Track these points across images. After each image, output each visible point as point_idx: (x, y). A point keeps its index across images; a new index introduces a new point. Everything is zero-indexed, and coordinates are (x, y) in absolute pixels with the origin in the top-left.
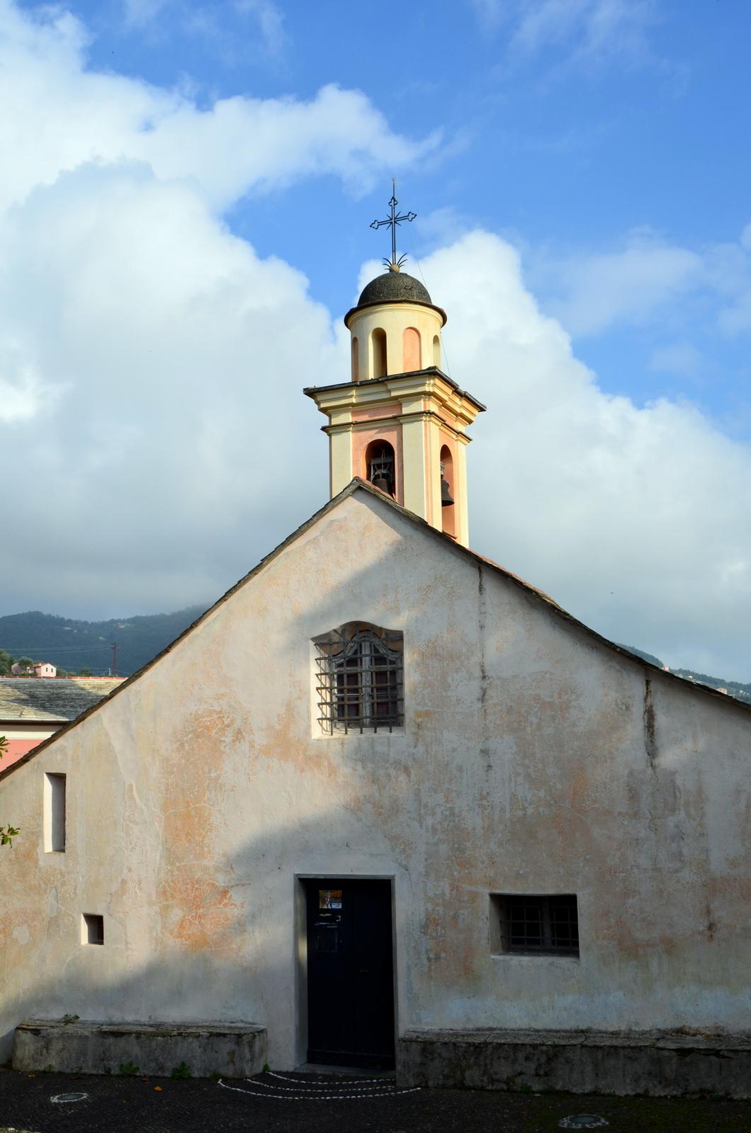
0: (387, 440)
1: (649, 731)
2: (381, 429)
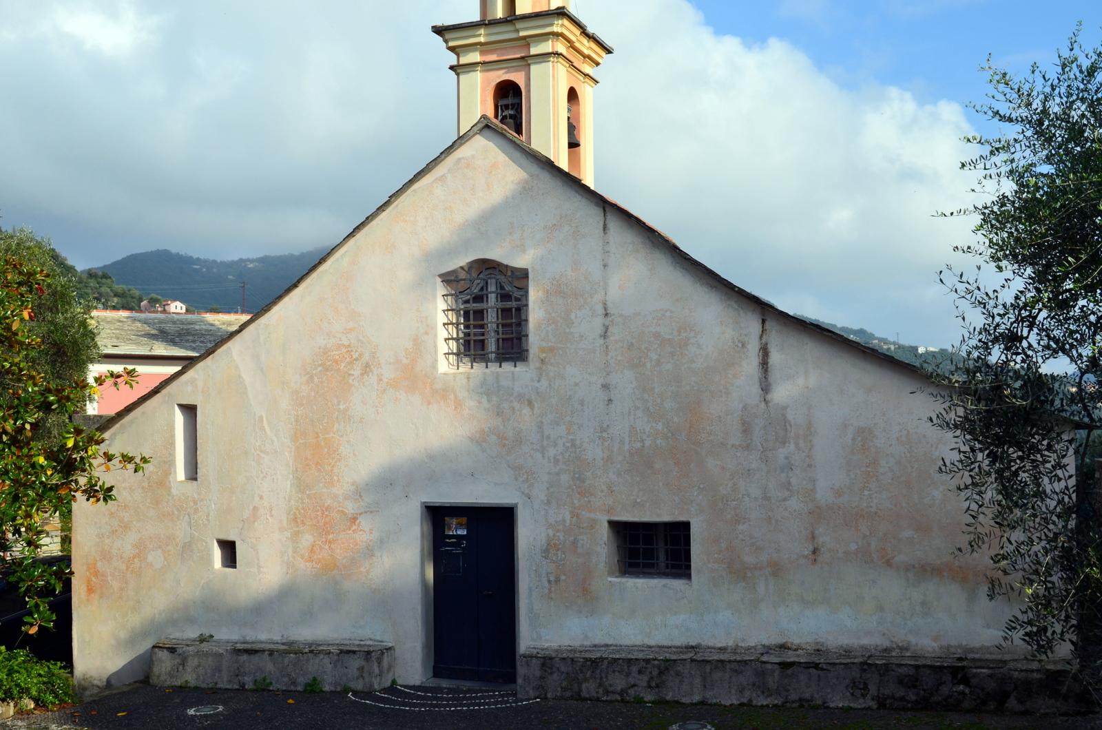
2: (509, 70)
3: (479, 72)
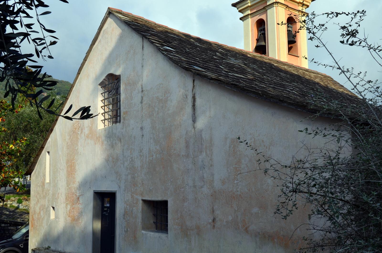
0: (262, 18)
1: (193, 107)
2: (260, 14)
3: (250, 18)
